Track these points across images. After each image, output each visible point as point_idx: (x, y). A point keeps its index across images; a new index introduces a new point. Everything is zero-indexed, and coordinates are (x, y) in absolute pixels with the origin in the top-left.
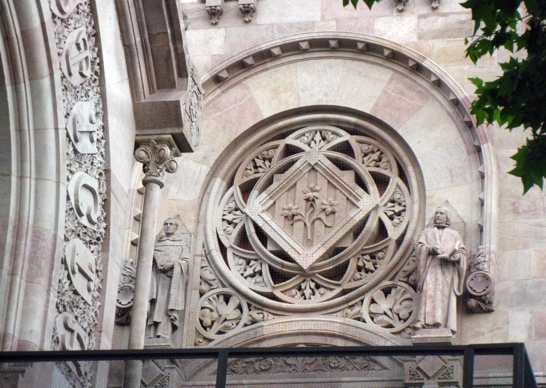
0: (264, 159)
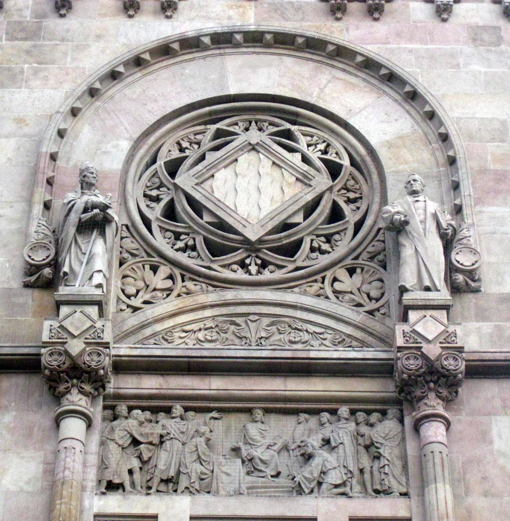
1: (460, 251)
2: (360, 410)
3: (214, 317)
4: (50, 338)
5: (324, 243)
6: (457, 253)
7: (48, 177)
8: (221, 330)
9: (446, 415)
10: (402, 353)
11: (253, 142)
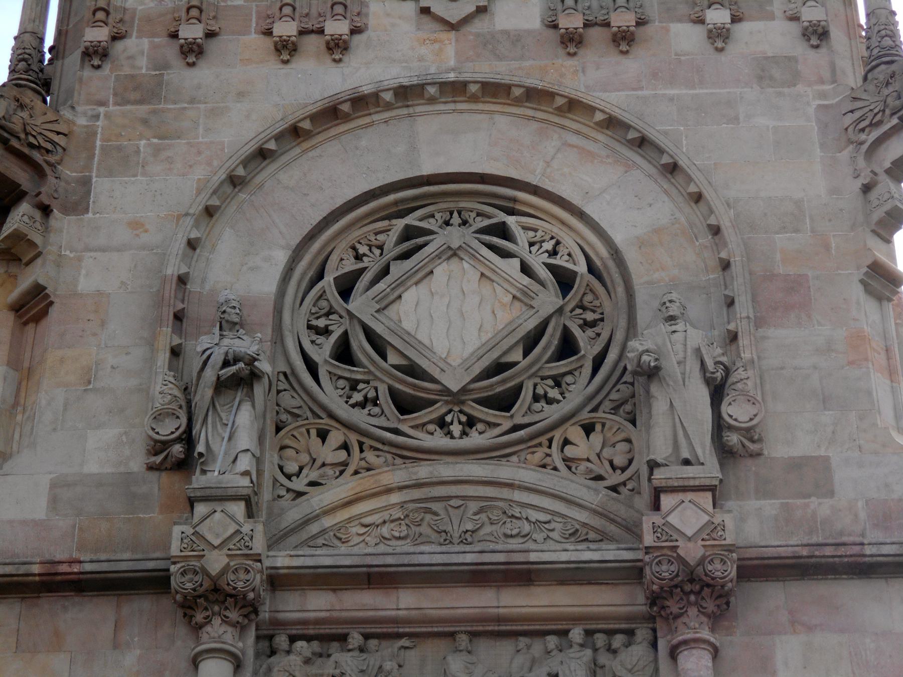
1: (734, 401)
2: (599, 631)
3: (402, 505)
4: (181, 551)
5: (552, 388)
6: (730, 404)
8: (412, 522)
9: (712, 640)
10: (651, 556)
11: (455, 245)
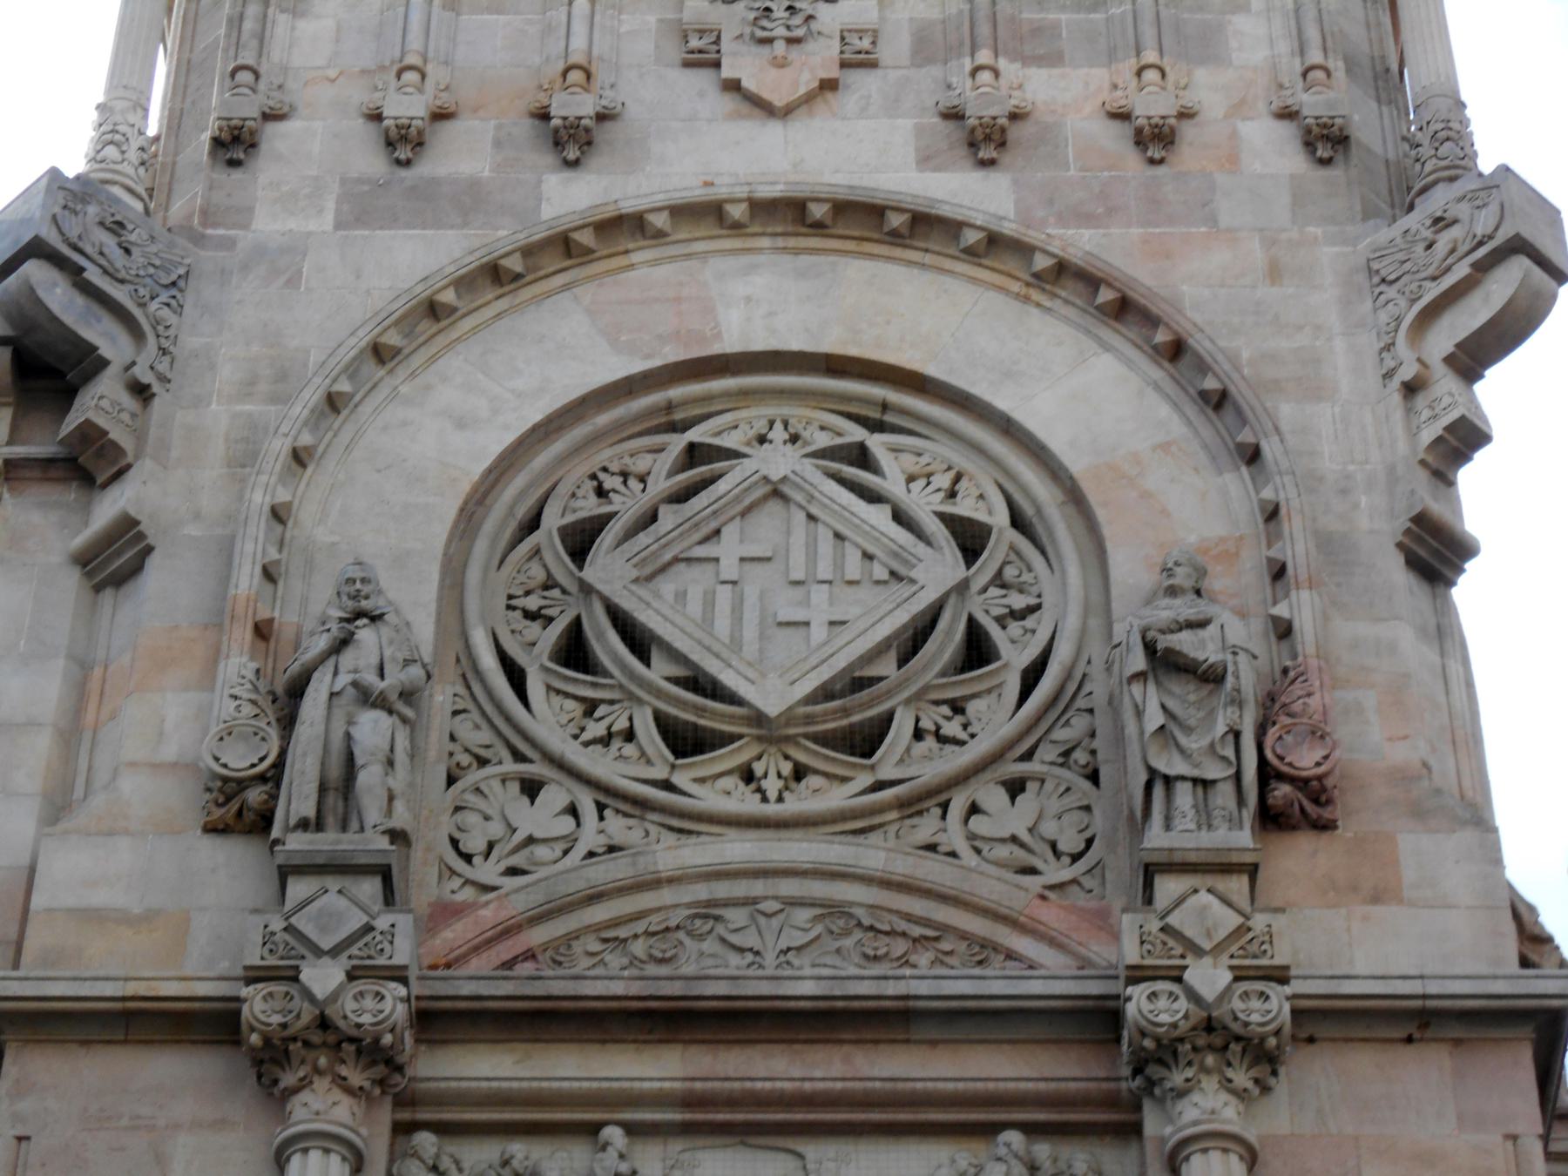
0: (625, 475)
7: (266, 560)
